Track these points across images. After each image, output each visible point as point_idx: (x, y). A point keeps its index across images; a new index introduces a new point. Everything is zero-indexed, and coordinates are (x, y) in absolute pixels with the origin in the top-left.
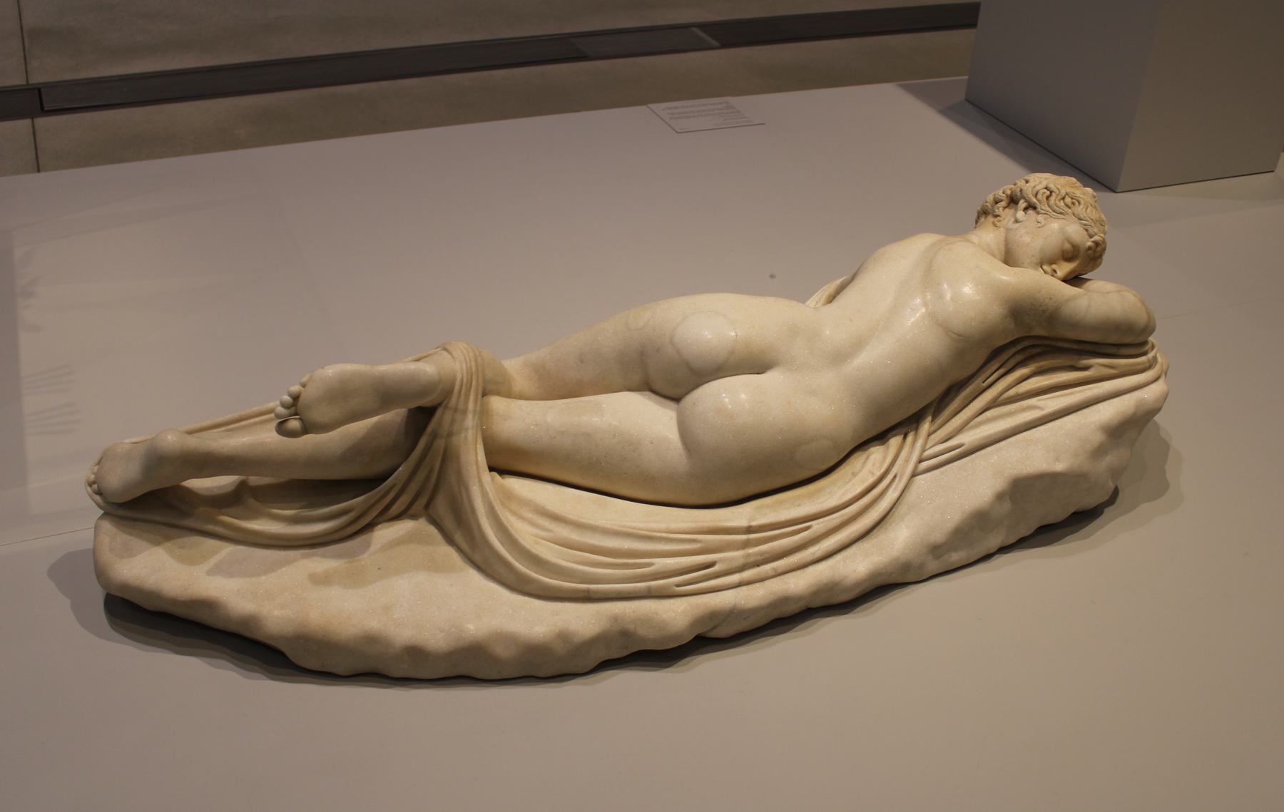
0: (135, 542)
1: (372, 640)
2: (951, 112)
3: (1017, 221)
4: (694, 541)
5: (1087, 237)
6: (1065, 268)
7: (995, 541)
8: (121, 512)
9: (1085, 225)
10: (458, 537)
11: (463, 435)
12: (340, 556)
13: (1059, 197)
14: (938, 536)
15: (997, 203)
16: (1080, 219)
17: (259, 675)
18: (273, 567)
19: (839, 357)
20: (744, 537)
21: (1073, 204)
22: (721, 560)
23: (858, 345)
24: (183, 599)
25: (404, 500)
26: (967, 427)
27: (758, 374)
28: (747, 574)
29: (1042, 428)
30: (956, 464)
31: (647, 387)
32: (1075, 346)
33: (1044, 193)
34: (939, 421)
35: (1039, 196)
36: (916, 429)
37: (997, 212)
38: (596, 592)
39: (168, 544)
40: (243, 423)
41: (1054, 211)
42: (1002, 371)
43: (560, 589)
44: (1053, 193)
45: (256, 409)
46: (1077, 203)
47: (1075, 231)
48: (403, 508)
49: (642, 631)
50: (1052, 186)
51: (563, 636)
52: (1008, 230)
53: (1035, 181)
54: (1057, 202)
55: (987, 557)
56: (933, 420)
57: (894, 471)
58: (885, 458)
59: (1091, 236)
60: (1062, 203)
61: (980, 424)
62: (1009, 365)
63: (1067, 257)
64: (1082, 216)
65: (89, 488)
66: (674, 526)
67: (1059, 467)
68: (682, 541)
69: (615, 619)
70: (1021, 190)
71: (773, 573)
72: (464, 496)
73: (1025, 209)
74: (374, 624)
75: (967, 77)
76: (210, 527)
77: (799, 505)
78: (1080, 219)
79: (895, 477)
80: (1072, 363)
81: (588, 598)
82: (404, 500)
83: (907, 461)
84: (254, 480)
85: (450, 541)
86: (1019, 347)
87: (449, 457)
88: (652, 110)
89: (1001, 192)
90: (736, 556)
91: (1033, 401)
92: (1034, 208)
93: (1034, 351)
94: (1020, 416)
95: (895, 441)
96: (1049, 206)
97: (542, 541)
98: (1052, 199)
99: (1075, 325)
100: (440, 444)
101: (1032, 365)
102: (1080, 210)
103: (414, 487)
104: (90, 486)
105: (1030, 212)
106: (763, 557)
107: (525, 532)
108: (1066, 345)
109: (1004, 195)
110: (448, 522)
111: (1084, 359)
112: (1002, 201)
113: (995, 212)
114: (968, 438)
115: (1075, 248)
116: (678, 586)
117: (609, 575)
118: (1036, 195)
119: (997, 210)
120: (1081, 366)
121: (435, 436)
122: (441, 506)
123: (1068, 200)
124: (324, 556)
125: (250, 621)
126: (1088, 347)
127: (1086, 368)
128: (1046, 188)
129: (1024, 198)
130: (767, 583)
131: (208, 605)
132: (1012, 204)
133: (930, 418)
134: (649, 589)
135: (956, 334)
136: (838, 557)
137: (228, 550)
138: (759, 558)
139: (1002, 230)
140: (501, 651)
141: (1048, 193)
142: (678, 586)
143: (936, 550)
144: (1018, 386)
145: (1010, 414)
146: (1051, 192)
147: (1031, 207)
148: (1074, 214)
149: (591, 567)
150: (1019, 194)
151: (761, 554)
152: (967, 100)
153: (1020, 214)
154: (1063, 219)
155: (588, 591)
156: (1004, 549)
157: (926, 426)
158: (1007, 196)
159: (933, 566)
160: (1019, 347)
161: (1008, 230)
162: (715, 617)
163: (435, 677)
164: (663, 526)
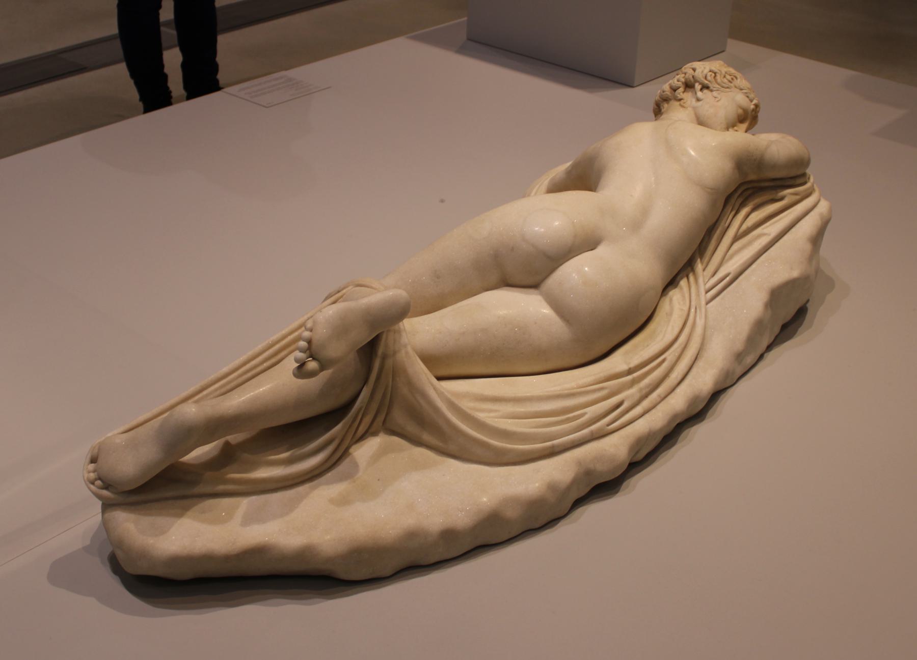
0: (161, 520)
1: (412, 535)
2: (462, 50)
3: (698, 100)
4: (602, 389)
5: (749, 102)
6: (744, 126)
7: (765, 342)
8: (134, 498)
9: (746, 93)
10: (426, 437)
11: (403, 352)
12: (341, 479)
13: (722, 76)
14: (739, 346)
15: (675, 91)
16: (741, 89)
17: (318, 600)
18: (291, 507)
19: (636, 225)
20: (630, 377)
21: (732, 79)
22: (627, 397)
23: (645, 212)
24: (235, 553)
25: (367, 420)
26: (725, 260)
27: (592, 250)
28: (646, 404)
29: (772, 249)
30: (728, 289)
31: (506, 283)
32: (771, 184)
33: (711, 75)
34: (706, 259)
35: (709, 78)
36: (693, 270)
37: (680, 97)
38: (559, 445)
39: (189, 513)
40: (205, 393)
41: (723, 87)
42: (733, 213)
43: (523, 453)
44: (717, 74)
45: (213, 377)
46: (734, 78)
47: (741, 98)
48: (366, 429)
49: (600, 467)
50: (713, 69)
51: (552, 487)
52: (694, 108)
53: (701, 68)
54: (723, 80)
55: (761, 357)
56: (701, 259)
57: (693, 303)
58: (683, 296)
59: (751, 101)
60: (725, 80)
61: (731, 257)
62: (736, 207)
63: (741, 119)
64: (742, 87)
65: (92, 486)
66: (581, 382)
67: (795, 274)
68: (594, 391)
69: (579, 463)
70: (693, 77)
71: (659, 399)
72: (422, 401)
73: (701, 90)
74: (409, 521)
75: (465, 19)
76: (221, 488)
77: (648, 346)
78: (741, 89)
79: (696, 308)
80: (771, 197)
81: (552, 453)
82: (367, 420)
83: (698, 295)
84: (235, 438)
85: (417, 442)
86: (739, 192)
87: (398, 372)
88: (227, 93)
89: (675, 80)
90: (632, 393)
91: (759, 230)
92: (708, 88)
93: (749, 192)
94: (756, 243)
95: (683, 283)
96: (719, 84)
97: (499, 420)
98: (718, 77)
99: (774, 166)
100: (389, 363)
101: (750, 204)
102: (738, 82)
103: (374, 406)
104: (93, 483)
105: (705, 91)
106: (649, 389)
107: (491, 416)
108: (767, 184)
109: (679, 83)
110: (411, 428)
111: (780, 192)
112: (679, 88)
113: (678, 97)
114: (732, 266)
115: (745, 111)
116: (608, 425)
117: (563, 433)
118: (706, 78)
119: (678, 95)
120: (779, 198)
121: (385, 357)
122: (399, 417)
123: (728, 77)
124: (329, 483)
125: (305, 553)
126: (779, 183)
127: (782, 199)
128: (710, 71)
129: (698, 82)
130: (658, 407)
131: (258, 551)
132: (687, 89)
133: (699, 260)
134: (592, 433)
135: (709, 188)
136: (689, 377)
137: (245, 503)
138: (647, 390)
139: (690, 109)
140: (511, 513)
141: (713, 75)
142: (608, 425)
143: (739, 357)
144: (746, 222)
145: (749, 243)
146: (715, 73)
147: (705, 87)
148: (736, 87)
149: (547, 427)
150: (692, 79)
151: (647, 386)
152: (469, 39)
153: (699, 94)
154: (731, 91)
155: (553, 447)
156: (769, 348)
157: (699, 266)
158: (683, 83)
159: (739, 371)
160: (739, 192)
161: (694, 108)
162: (639, 442)
163: (461, 553)
164: (573, 384)
